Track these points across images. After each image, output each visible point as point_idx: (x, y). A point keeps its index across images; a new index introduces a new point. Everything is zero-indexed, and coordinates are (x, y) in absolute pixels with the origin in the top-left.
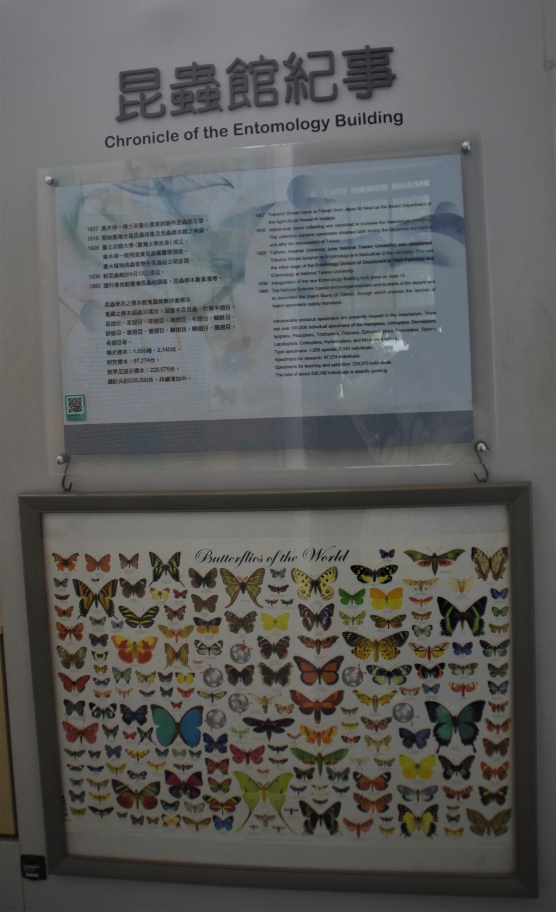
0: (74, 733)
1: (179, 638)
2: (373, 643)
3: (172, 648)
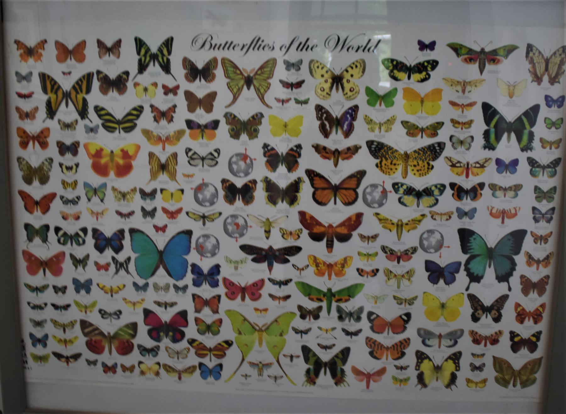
0: (36, 265)
1: (167, 145)
2: (402, 155)
3: (157, 157)
